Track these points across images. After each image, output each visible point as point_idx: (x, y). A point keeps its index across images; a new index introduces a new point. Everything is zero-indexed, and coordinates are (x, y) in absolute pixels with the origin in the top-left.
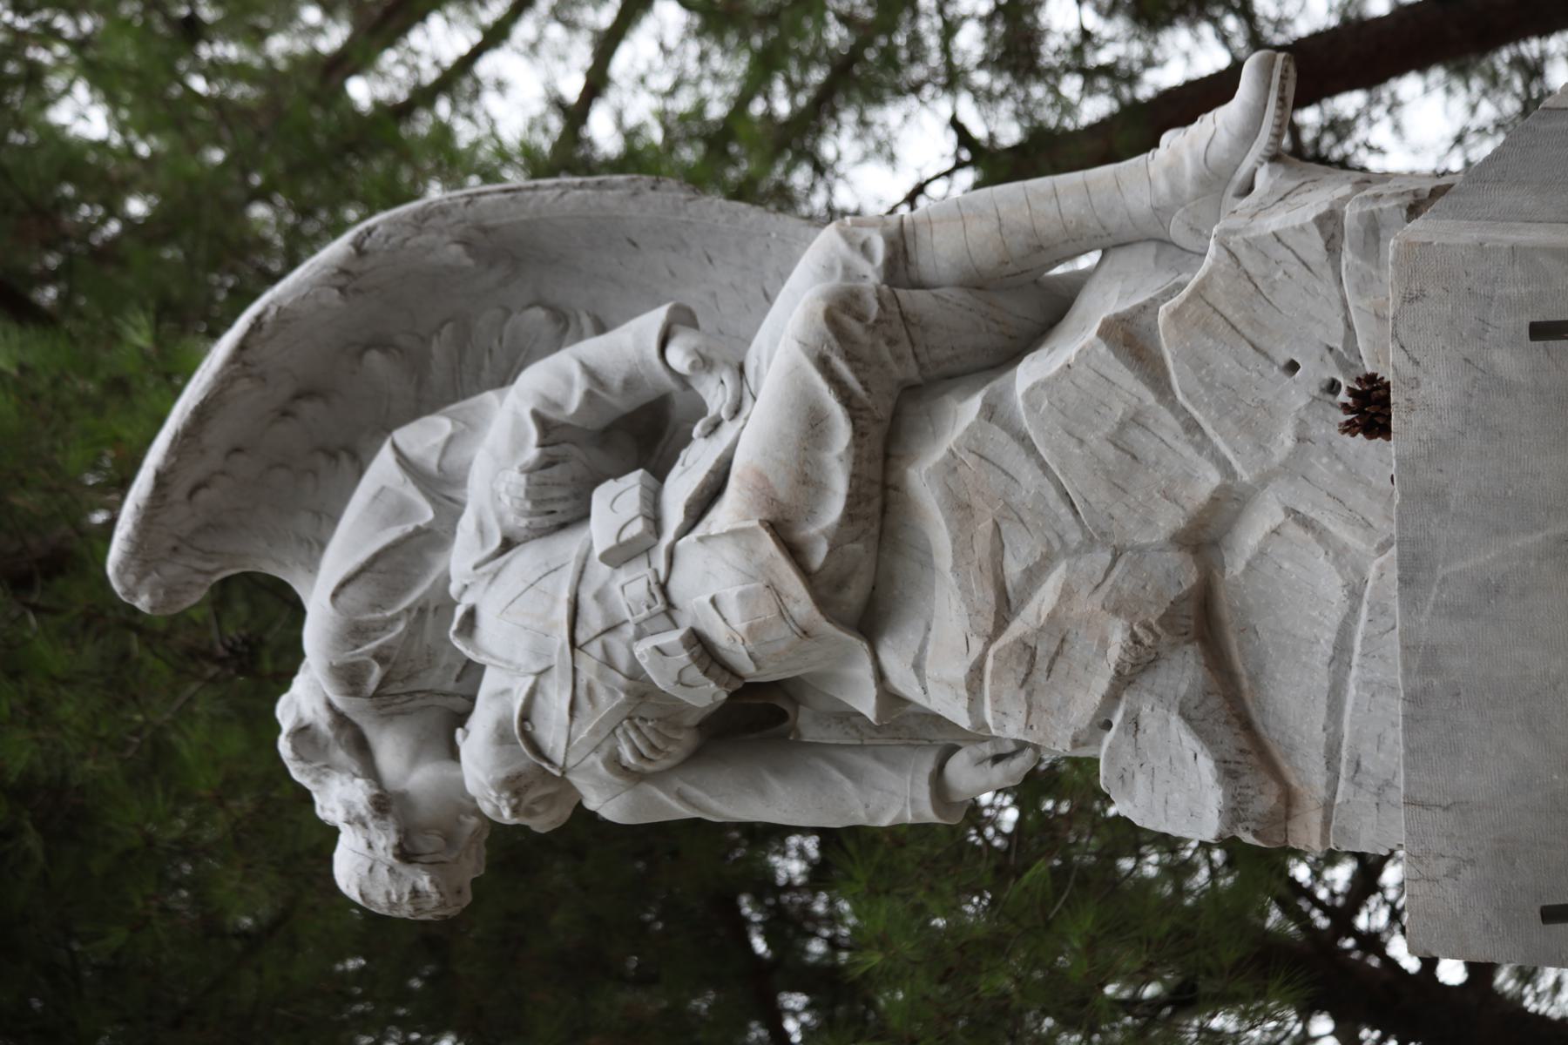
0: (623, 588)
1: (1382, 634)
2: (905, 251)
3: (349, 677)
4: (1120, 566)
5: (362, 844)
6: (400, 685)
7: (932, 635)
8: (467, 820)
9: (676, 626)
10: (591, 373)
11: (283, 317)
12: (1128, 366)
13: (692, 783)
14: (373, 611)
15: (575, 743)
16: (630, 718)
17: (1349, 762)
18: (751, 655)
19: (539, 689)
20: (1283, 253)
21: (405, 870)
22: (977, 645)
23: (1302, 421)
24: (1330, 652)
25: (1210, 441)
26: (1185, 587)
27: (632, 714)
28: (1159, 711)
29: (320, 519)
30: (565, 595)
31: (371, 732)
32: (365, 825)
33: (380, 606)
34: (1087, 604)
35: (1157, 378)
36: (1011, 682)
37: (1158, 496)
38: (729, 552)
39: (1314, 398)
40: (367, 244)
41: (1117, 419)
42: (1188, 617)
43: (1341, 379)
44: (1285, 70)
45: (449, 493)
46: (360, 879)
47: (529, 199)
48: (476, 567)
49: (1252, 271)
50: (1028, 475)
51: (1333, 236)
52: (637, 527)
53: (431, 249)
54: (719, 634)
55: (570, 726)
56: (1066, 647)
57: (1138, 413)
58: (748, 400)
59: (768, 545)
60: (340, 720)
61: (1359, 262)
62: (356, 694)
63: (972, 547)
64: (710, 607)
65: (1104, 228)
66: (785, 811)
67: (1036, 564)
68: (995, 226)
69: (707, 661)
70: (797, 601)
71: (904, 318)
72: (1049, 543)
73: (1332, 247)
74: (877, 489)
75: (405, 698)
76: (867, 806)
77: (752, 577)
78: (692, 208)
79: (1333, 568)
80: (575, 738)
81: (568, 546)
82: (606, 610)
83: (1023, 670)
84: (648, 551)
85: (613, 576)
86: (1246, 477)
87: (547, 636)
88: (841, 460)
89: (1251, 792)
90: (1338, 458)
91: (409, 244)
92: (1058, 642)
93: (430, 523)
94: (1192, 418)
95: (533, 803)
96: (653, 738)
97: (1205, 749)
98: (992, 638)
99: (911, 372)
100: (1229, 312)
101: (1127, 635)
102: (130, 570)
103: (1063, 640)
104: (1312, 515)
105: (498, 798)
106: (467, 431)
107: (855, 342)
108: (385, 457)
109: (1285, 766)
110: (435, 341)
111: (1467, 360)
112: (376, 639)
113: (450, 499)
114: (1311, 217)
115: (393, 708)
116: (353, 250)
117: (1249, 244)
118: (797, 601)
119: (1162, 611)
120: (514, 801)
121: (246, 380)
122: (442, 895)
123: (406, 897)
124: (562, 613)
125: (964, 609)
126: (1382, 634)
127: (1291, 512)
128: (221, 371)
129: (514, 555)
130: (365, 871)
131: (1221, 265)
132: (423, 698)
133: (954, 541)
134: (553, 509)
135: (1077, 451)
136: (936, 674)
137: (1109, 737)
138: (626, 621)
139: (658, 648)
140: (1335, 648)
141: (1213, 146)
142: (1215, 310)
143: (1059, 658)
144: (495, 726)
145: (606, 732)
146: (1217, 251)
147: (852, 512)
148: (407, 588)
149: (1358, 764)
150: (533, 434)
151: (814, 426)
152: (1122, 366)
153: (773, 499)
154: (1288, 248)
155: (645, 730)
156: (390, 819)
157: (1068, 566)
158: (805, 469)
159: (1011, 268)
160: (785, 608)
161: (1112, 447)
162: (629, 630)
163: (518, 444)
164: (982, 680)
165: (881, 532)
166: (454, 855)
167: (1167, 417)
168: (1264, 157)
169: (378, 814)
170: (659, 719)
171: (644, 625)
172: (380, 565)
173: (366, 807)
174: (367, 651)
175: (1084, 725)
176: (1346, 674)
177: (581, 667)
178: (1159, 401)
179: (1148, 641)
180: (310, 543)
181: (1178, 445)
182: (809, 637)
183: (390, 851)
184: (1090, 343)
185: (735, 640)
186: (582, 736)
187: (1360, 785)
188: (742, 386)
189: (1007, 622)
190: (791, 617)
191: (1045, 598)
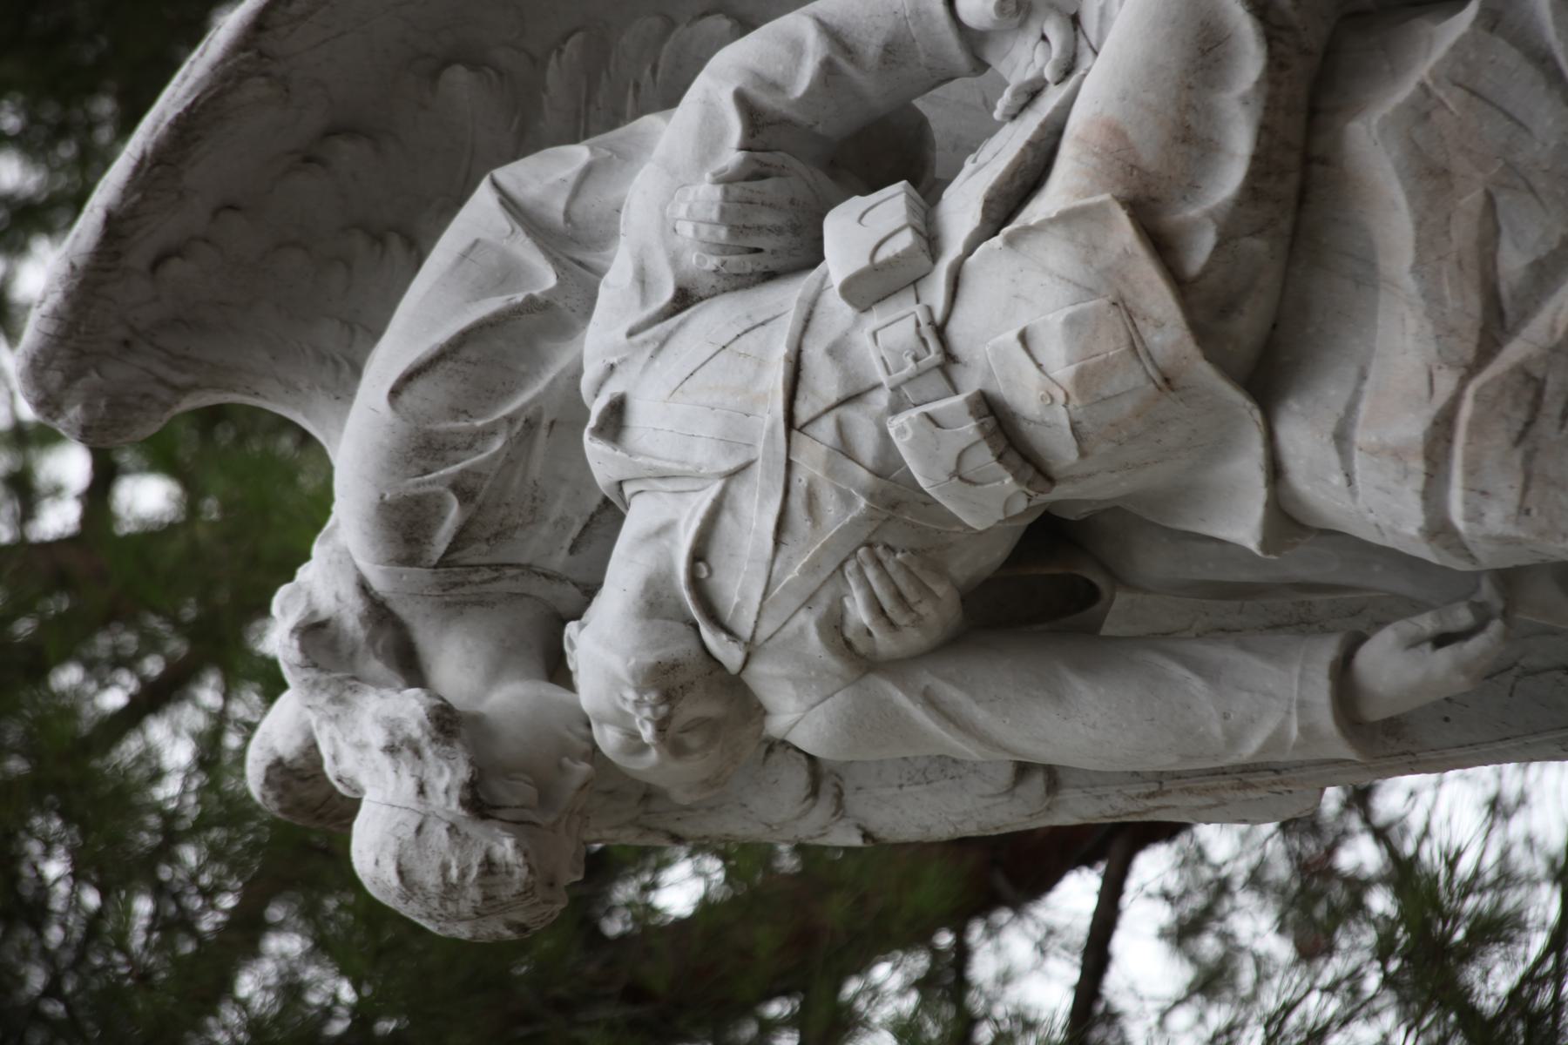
0: (874, 334)
5: (409, 785)
6: (484, 547)
7: (1367, 387)
8: (577, 767)
9: (956, 392)
13: (949, 679)
14: (456, 419)
16: (870, 545)
18: (1074, 427)
19: (726, 503)
21: (475, 830)
22: (1446, 383)
27: (874, 539)
29: (352, 331)
31: (425, 636)
32: (418, 753)
33: (465, 412)
36: (1500, 437)
38: (1055, 254)
44: (931, 702)
45: (578, 256)
46: (401, 845)
48: (631, 333)
52: (906, 240)
55: (773, 561)
58: (1086, 59)
59: (1123, 233)
60: (379, 611)
62: (411, 561)
63: (1447, 233)
64: (1018, 345)
66: (1094, 726)
67: (1553, 253)
69: (1002, 444)
70: (1159, 325)
75: (487, 574)
76: (1226, 716)
77: (1090, 290)
80: (779, 581)
81: (788, 296)
82: (845, 369)
83: (1521, 416)
84: (915, 283)
85: (857, 323)
87: (747, 415)
88: (1246, 103)
93: (550, 292)
98: (1472, 370)
102: (55, 364)
105: (638, 704)
108: (484, 196)
110: (553, 62)
112: (456, 462)
113: (580, 264)
115: (467, 590)
118: (1159, 325)
121: (262, 80)
122: (531, 871)
123: (474, 872)
124: (775, 378)
125: (1429, 328)
128: (223, 61)
129: (694, 313)
130: (408, 833)
133: (1419, 225)
134: (760, 246)
136: (1374, 439)
139: (929, 416)
144: (642, 587)
147: (1257, 185)
148: (509, 392)
150: (735, 128)
153: (1133, 167)
155: (891, 566)
156: (458, 746)
158: (1187, 117)
160: (1140, 338)
162: (882, 399)
163: (709, 143)
164: (1450, 441)
166: (551, 818)
169: (441, 736)
170: (914, 551)
171: (905, 390)
172: (469, 352)
173: (422, 725)
180: (336, 363)
182: (1173, 390)
183: (455, 795)
185: (1052, 399)
186: (789, 577)
188: (1076, 39)
190: (1149, 353)
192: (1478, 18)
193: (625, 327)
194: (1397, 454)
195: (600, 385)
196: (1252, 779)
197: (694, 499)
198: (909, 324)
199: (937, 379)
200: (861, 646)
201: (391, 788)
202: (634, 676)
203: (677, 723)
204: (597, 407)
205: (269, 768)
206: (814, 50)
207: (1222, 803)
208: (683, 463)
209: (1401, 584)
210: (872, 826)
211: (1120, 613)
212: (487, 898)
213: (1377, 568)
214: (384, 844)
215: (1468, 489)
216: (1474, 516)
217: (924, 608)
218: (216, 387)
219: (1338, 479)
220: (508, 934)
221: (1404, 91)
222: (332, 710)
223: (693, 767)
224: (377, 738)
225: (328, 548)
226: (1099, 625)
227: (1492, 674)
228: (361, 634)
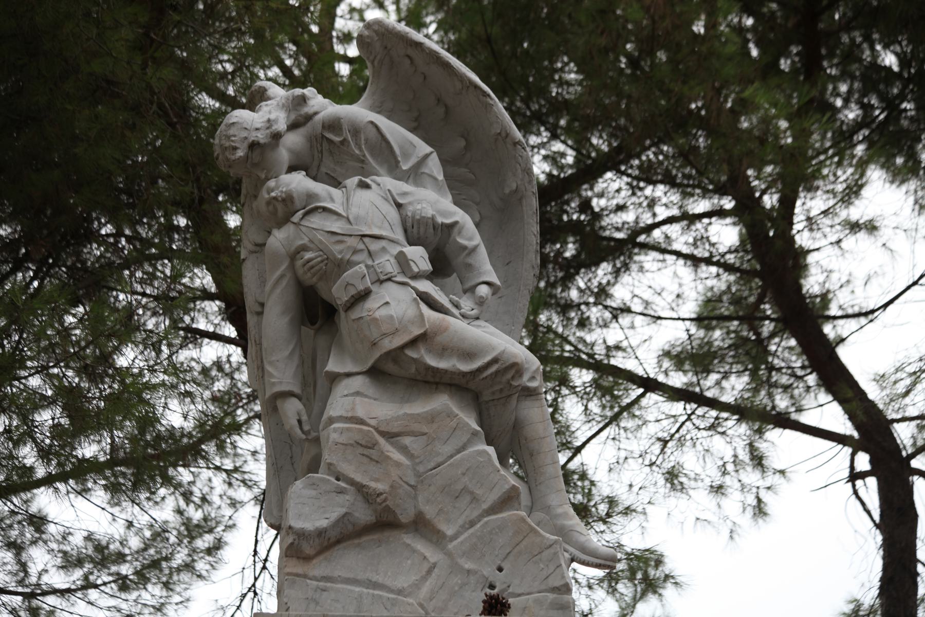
1: (383, 603)
2: (531, 395)
3: (334, 125)
4: (409, 488)
5: (259, 126)
7: (372, 401)
10: (475, 249)
11: (489, 107)
12: (499, 497)
16: (327, 259)
17: (326, 586)
18: (361, 318)
20: (552, 568)
21: (246, 145)
23: (476, 573)
24: (374, 580)
26: (400, 517)
30: (383, 233)
31: (302, 131)
32: (268, 128)
34: (394, 473)
36: (358, 437)
38: (411, 312)
39: (487, 579)
40: (519, 147)
44: (282, 276)
48: (389, 190)
49: (543, 554)
50: (447, 449)
51: (560, 590)
52: (416, 269)
54: (371, 304)
56: (374, 463)
57: (478, 500)
58: (467, 321)
59: (417, 331)
60: (309, 118)
61: (549, 601)
62: (323, 127)
70: (390, 342)
71: (510, 396)
73: (555, 590)
74: (437, 380)
78: (526, 292)
81: (400, 236)
83: (363, 443)
84: (403, 272)
85: (392, 255)
86: (451, 546)
89: (311, 542)
90: (461, 587)
92: (376, 459)
94: (476, 524)
95: (274, 206)
96: (317, 268)
97: (330, 524)
98: (376, 429)
99: (486, 396)
100: (524, 543)
103: (377, 462)
104: (433, 575)
105: (282, 192)
106: (439, 190)
108: (428, 149)
109: (321, 557)
115: (315, 143)
117: (556, 554)
118: (390, 342)
119: (391, 507)
120: (280, 199)
122: (234, 161)
123: (233, 144)
124: (376, 232)
127: (434, 566)
128: (466, 76)
133: (418, 415)
137: (333, 479)
138: (374, 261)
139: (365, 276)
140: (375, 582)
142: (525, 537)
148: (372, 155)
149: (324, 591)
151: (468, 354)
152: (499, 494)
155: (321, 265)
162: (370, 262)
163: (444, 214)
164: (356, 423)
165: (416, 380)
167: (476, 513)
171: (372, 269)
172: (384, 144)
173: (276, 129)
174: (347, 135)
175: (339, 468)
176: (363, 587)
178: (484, 510)
179: (378, 500)
181: (463, 517)
183: (256, 139)
187: (316, 591)
189: (383, 437)
191: (396, 455)
193: (391, 189)
194: (353, 409)
196: (260, 370)
197: (341, 208)
198: (391, 270)
199: (376, 278)
200: (298, 256)
203: (277, 204)
204: (368, 180)
205: (264, 88)
206: (470, 244)
210: (246, 262)
211: (308, 331)
212: (226, 148)
215: (343, 428)
216: (335, 430)
217: (309, 274)
219: (346, 392)
220: (216, 154)
221: (456, 410)
222: (281, 104)
223: (263, 208)
224: (272, 117)
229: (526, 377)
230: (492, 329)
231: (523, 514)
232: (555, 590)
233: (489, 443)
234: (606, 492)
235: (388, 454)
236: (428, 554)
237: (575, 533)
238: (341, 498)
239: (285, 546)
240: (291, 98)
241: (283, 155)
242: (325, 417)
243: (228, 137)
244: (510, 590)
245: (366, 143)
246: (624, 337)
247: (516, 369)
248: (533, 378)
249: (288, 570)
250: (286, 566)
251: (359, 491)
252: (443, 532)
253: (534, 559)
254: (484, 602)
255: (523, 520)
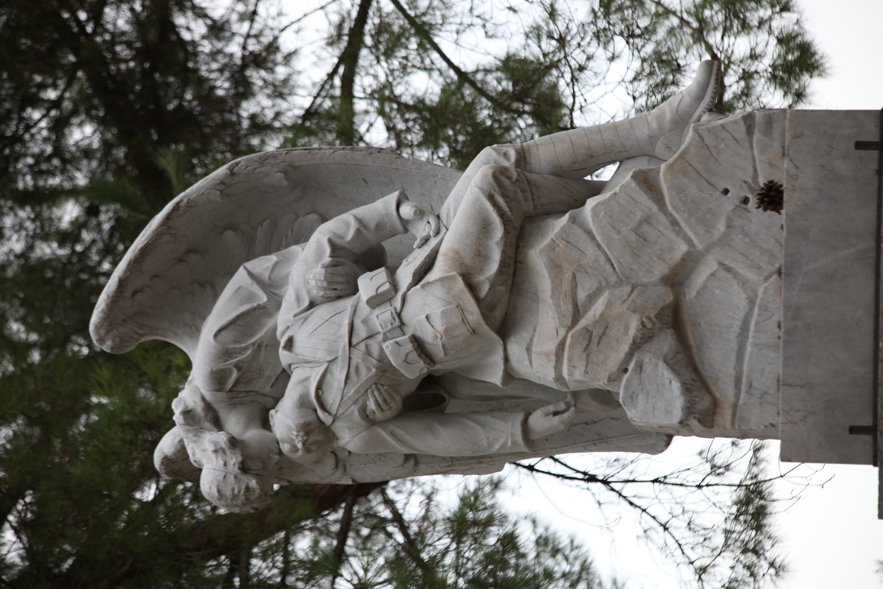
0: (377, 316)
1: (765, 320)
2: (525, 157)
3: (218, 379)
5: (221, 463)
6: (244, 386)
7: (536, 333)
9: (404, 335)
10: (359, 220)
11: (191, 204)
12: (646, 193)
14: (235, 344)
15: (345, 399)
16: (376, 384)
18: (443, 346)
20: (725, 135)
21: (243, 477)
22: (562, 332)
24: (738, 331)
25: (683, 230)
26: (667, 302)
28: (654, 360)
30: (346, 322)
31: (223, 414)
32: (224, 452)
34: (619, 308)
35: (659, 199)
36: (579, 349)
37: (655, 258)
38: (438, 291)
39: (737, 206)
40: (236, 169)
41: (638, 220)
42: (668, 316)
43: (750, 196)
44: (393, 435)
45: (273, 291)
47: (317, 154)
48: (295, 316)
50: (591, 251)
52: (387, 286)
53: (267, 175)
54: (428, 335)
56: (608, 331)
58: (443, 230)
59: (460, 284)
60: (208, 407)
61: (762, 138)
62: (220, 390)
63: (561, 285)
65: (624, 147)
67: (594, 292)
68: (570, 145)
70: (472, 314)
71: (528, 182)
72: (600, 282)
73: (750, 131)
74: (512, 262)
75: (244, 394)
76: (488, 438)
79: (741, 290)
81: (347, 304)
83: (585, 343)
84: (390, 300)
85: (371, 313)
86: (700, 246)
89: (697, 399)
91: (257, 171)
92: (604, 328)
93: (265, 303)
95: (311, 444)
97: (677, 379)
98: (570, 328)
99: (529, 207)
100: (696, 165)
101: (639, 323)
103: (607, 327)
104: (732, 265)
105: (297, 436)
107: (506, 189)
108: (241, 273)
109: (714, 388)
110: (259, 228)
111: (822, 166)
113: (274, 293)
114: (740, 117)
115: (238, 399)
116: (229, 172)
117: (709, 131)
118: (472, 314)
119: (657, 312)
120: (305, 438)
121: (168, 236)
122: (261, 490)
125: (556, 315)
126: (765, 320)
127: (721, 264)
128: (156, 230)
130: (221, 478)
131: (694, 142)
132: (253, 395)
133: (552, 283)
135: (617, 237)
137: (626, 377)
138: (379, 333)
139: (396, 342)
140: (741, 329)
141: (681, 104)
142: (690, 165)
143: (604, 337)
145: (363, 391)
146: (693, 135)
148: (252, 335)
150: (328, 250)
151: (485, 227)
154: (728, 132)
155: (382, 391)
156: (237, 450)
157: (610, 293)
159: (577, 166)
161: (634, 234)
162: (380, 337)
163: (319, 255)
164: (563, 350)
168: (706, 109)
170: (390, 386)
171: (388, 334)
172: (240, 322)
173: (225, 443)
175: (614, 370)
177: (354, 357)
179: (649, 326)
180: (190, 326)
181: (667, 232)
183: (237, 466)
184: (627, 182)
187: (751, 394)
189: (578, 321)
191: (599, 307)
192: (569, 219)
193: (293, 314)
194: (547, 355)
195: (284, 333)
196: (483, 460)
197: (317, 369)
198: (389, 313)
199: (398, 331)
200: (371, 417)
201: (214, 464)
202: (297, 427)
203: (310, 441)
204: (283, 341)
205: (163, 459)
206: (354, 226)
207: (473, 468)
208: (314, 357)
209: (542, 396)
210: (355, 478)
211: (452, 406)
212: (247, 499)
213: (534, 391)
214: (212, 482)
215: (569, 365)
216: (571, 374)
217: (392, 404)
218: (152, 334)
219: (527, 363)
220: (252, 511)
221: (546, 241)
222: (194, 439)
223: (313, 456)
224: (211, 448)
225: (191, 386)
226: (445, 410)
227: (571, 425)
228: (202, 414)
229: (506, 164)
230: (450, 201)
231: (663, 166)
232: (750, 131)
233: (583, 203)
234: (520, 40)
235: (597, 316)
236: (709, 271)
237: (681, 108)
238: (648, 367)
239: (701, 428)
240: (187, 427)
241: (252, 435)
242: (554, 386)
243: (235, 497)
244: (750, 180)
245: (240, 343)
246: (321, 12)
247: (499, 175)
248: (506, 155)
249: (728, 425)
250: (724, 428)
251: (639, 347)
252: (684, 255)
253: (714, 154)
254: (765, 209)
255: (670, 167)
